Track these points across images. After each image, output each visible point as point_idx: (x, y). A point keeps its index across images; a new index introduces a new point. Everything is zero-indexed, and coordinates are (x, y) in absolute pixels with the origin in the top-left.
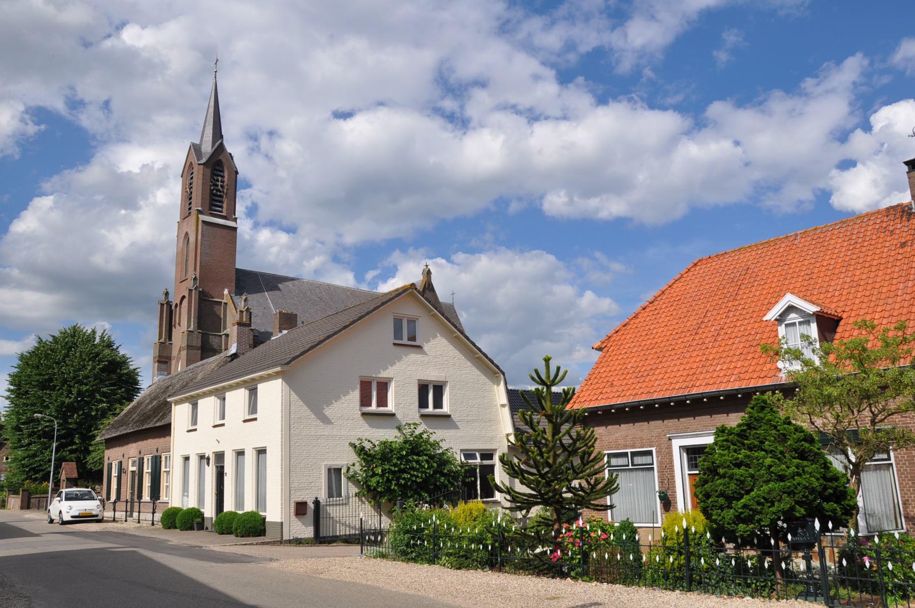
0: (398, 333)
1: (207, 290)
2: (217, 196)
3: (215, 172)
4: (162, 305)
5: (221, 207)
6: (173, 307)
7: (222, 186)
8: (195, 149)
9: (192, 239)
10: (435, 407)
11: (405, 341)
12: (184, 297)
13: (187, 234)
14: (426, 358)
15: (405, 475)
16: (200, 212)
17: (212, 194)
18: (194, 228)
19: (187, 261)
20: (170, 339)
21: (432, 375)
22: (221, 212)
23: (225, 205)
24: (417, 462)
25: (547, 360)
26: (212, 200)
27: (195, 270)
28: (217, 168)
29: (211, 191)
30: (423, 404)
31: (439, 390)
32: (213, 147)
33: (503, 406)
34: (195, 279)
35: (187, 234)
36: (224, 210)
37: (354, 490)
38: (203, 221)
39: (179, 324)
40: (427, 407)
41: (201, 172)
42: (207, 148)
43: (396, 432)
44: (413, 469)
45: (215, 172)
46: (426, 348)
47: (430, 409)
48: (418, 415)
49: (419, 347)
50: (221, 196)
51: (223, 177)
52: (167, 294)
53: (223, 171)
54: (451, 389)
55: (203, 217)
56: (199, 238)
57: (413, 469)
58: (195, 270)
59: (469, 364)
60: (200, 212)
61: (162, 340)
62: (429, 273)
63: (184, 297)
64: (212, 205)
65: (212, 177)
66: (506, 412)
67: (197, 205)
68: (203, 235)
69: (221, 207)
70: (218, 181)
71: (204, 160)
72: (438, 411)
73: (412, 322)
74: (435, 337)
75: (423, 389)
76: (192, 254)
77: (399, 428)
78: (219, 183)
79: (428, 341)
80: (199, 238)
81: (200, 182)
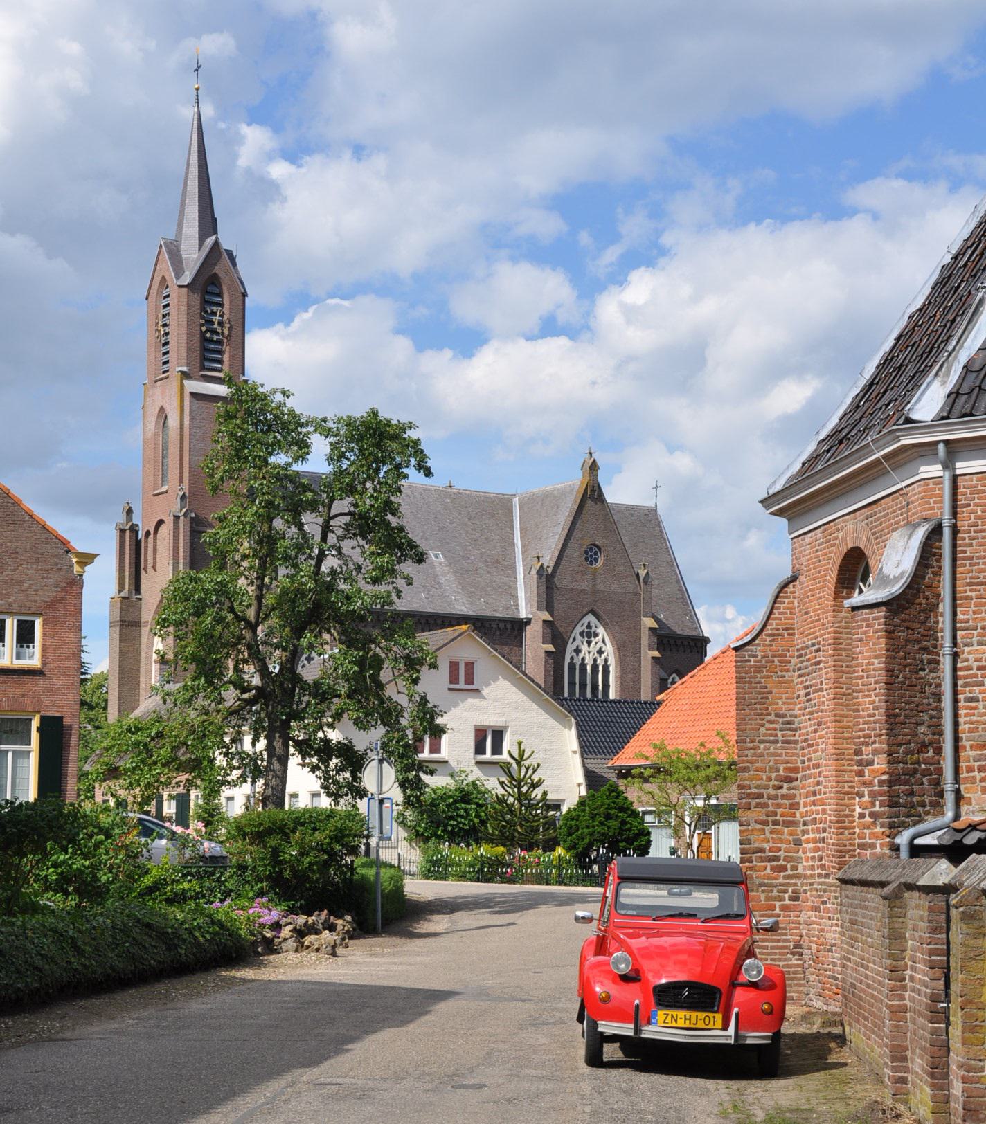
0: (454, 678)
1: (202, 514)
2: (211, 341)
3: (208, 298)
4: (122, 531)
5: (220, 361)
6: (141, 535)
7: (220, 323)
8: (169, 253)
9: (173, 422)
10: (493, 753)
11: (462, 685)
12: (161, 522)
13: (162, 409)
14: (484, 702)
15: (452, 822)
16: (185, 375)
17: (204, 339)
18: (176, 403)
19: (164, 457)
20: (138, 590)
21: (491, 720)
22: (220, 370)
23: (226, 358)
24: (466, 810)
25: (520, 744)
26: (204, 350)
27: (181, 481)
28: (210, 289)
29: (203, 334)
30: (480, 749)
31: (498, 735)
32: (200, 246)
33: (575, 752)
34: (183, 497)
35: (162, 409)
36: (226, 367)
37: (403, 834)
38: (192, 394)
39: (154, 568)
40: (484, 753)
41: (184, 300)
42: (193, 255)
43: (448, 780)
44: (461, 816)
45: (208, 298)
46: (485, 692)
47: (488, 756)
48: (473, 762)
49: (477, 691)
50: (219, 342)
51: (221, 305)
52: (129, 512)
53: (220, 295)
54: (513, 734)
55: (194, 386)
56: (187, 422)
57: (461, 816)
58: (181, 481)
59: (535, 706)
60: (185, 375)
61: (125, 593)
62: (594, 467)
63: (161, 522)
64: (204, 359)
65: (203, 310)
66: (578, 757)
67: (178, 366)
68: (192, 419)
69: (220, 361)
70: (214, 314)
71: (187, 278)
72: (497, 758)
73: (470, 666)
74: (496, 679)
75: (480, 735)
76: (174, 451)
77: (452, 775)
78: (216, 319)
79: (488, 685)
80: (187, 422)
81: (184, 319)
